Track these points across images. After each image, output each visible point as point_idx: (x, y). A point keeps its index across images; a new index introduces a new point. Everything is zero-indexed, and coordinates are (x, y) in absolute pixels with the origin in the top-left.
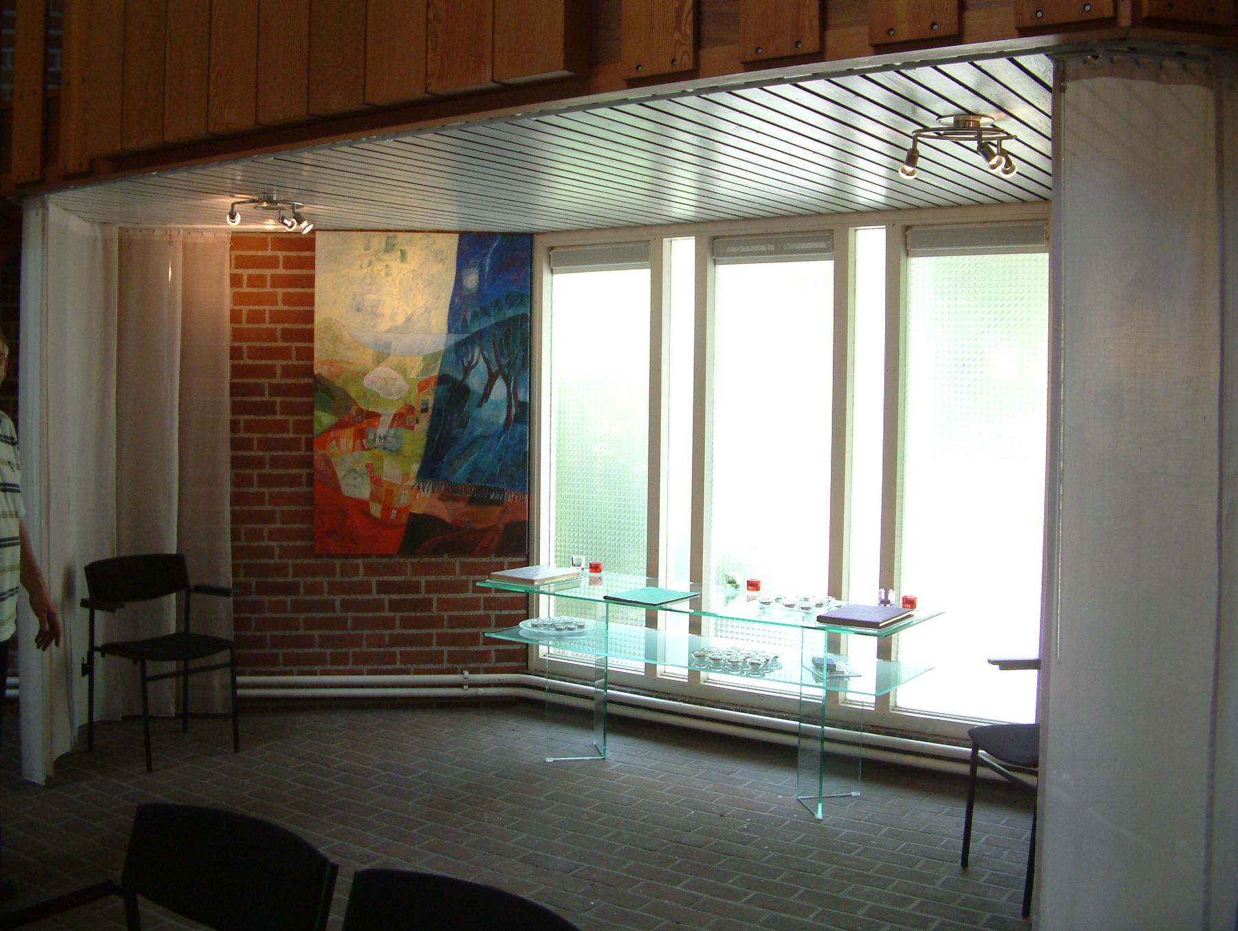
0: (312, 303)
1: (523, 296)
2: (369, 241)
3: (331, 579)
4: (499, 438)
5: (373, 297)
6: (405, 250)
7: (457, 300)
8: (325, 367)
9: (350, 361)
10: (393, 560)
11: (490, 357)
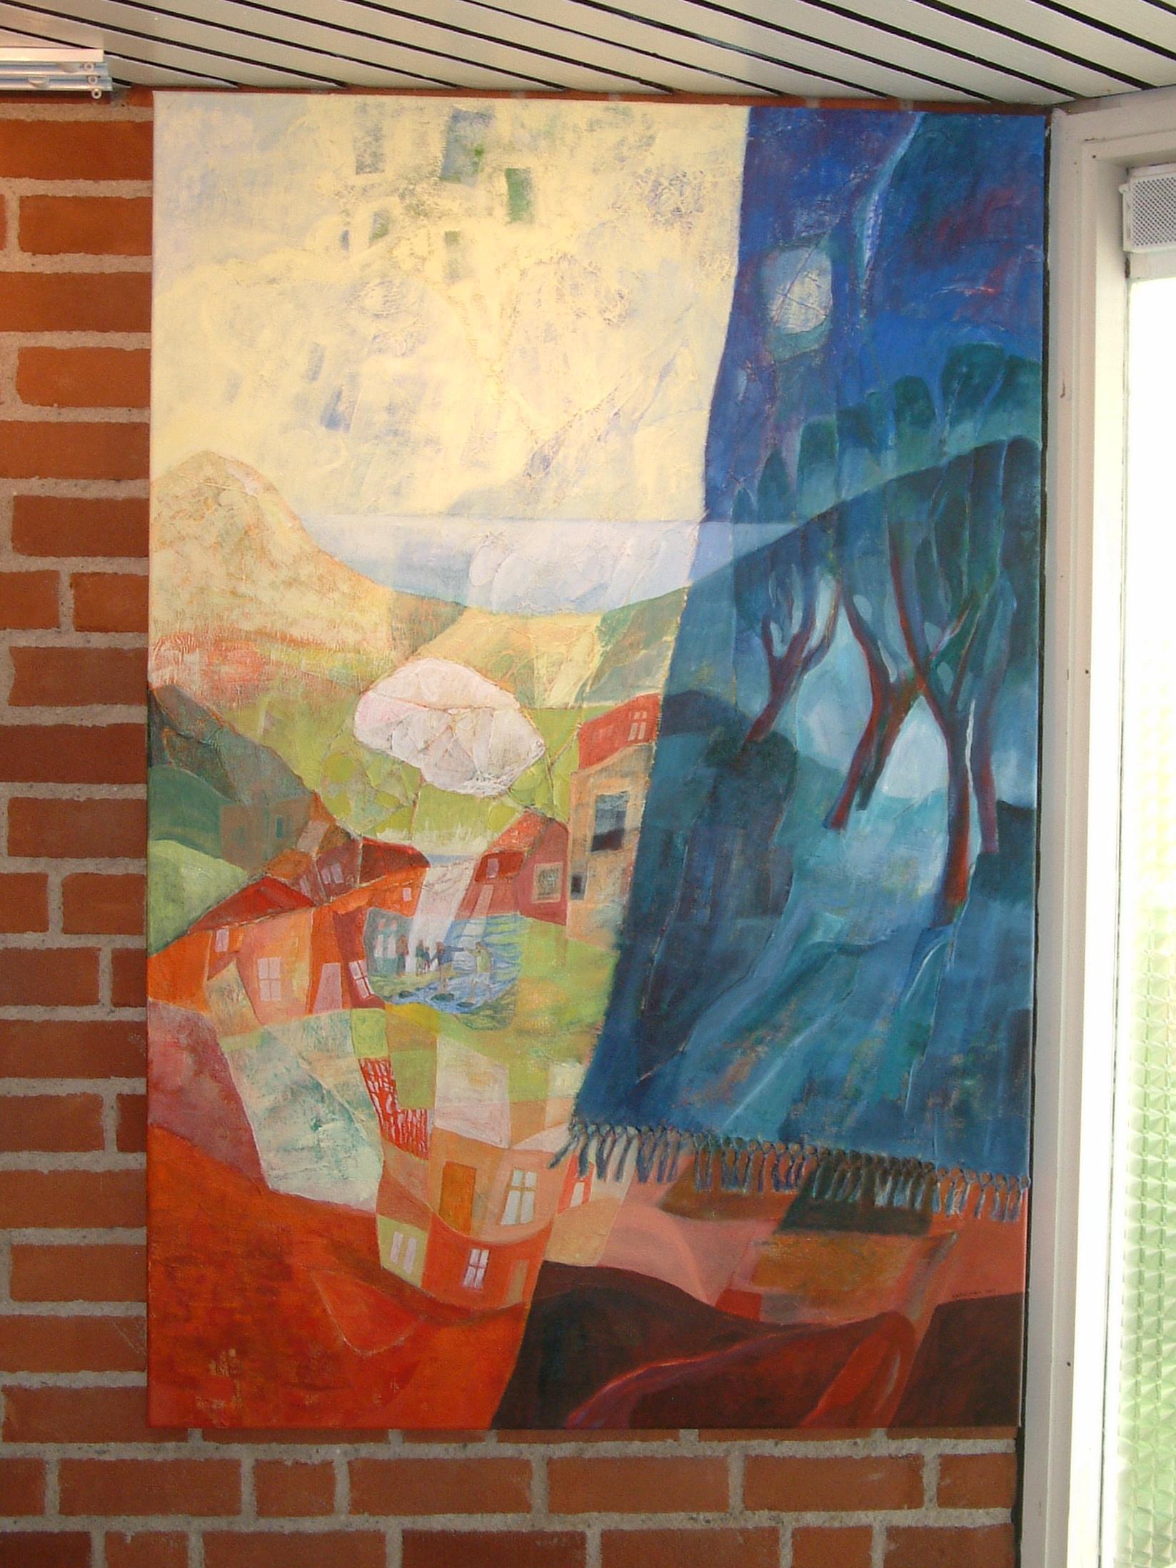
0: (139, 394)
1: (1014, 367)
2: (377, 135)
3: (219, 1524)
4: (918, 953)
5: (395, 366)
6: (527, 171)
7: (742, 380)
8: (194, 658)
9: (296, 632)
10: (475, 1450)
11: (879, 618)
